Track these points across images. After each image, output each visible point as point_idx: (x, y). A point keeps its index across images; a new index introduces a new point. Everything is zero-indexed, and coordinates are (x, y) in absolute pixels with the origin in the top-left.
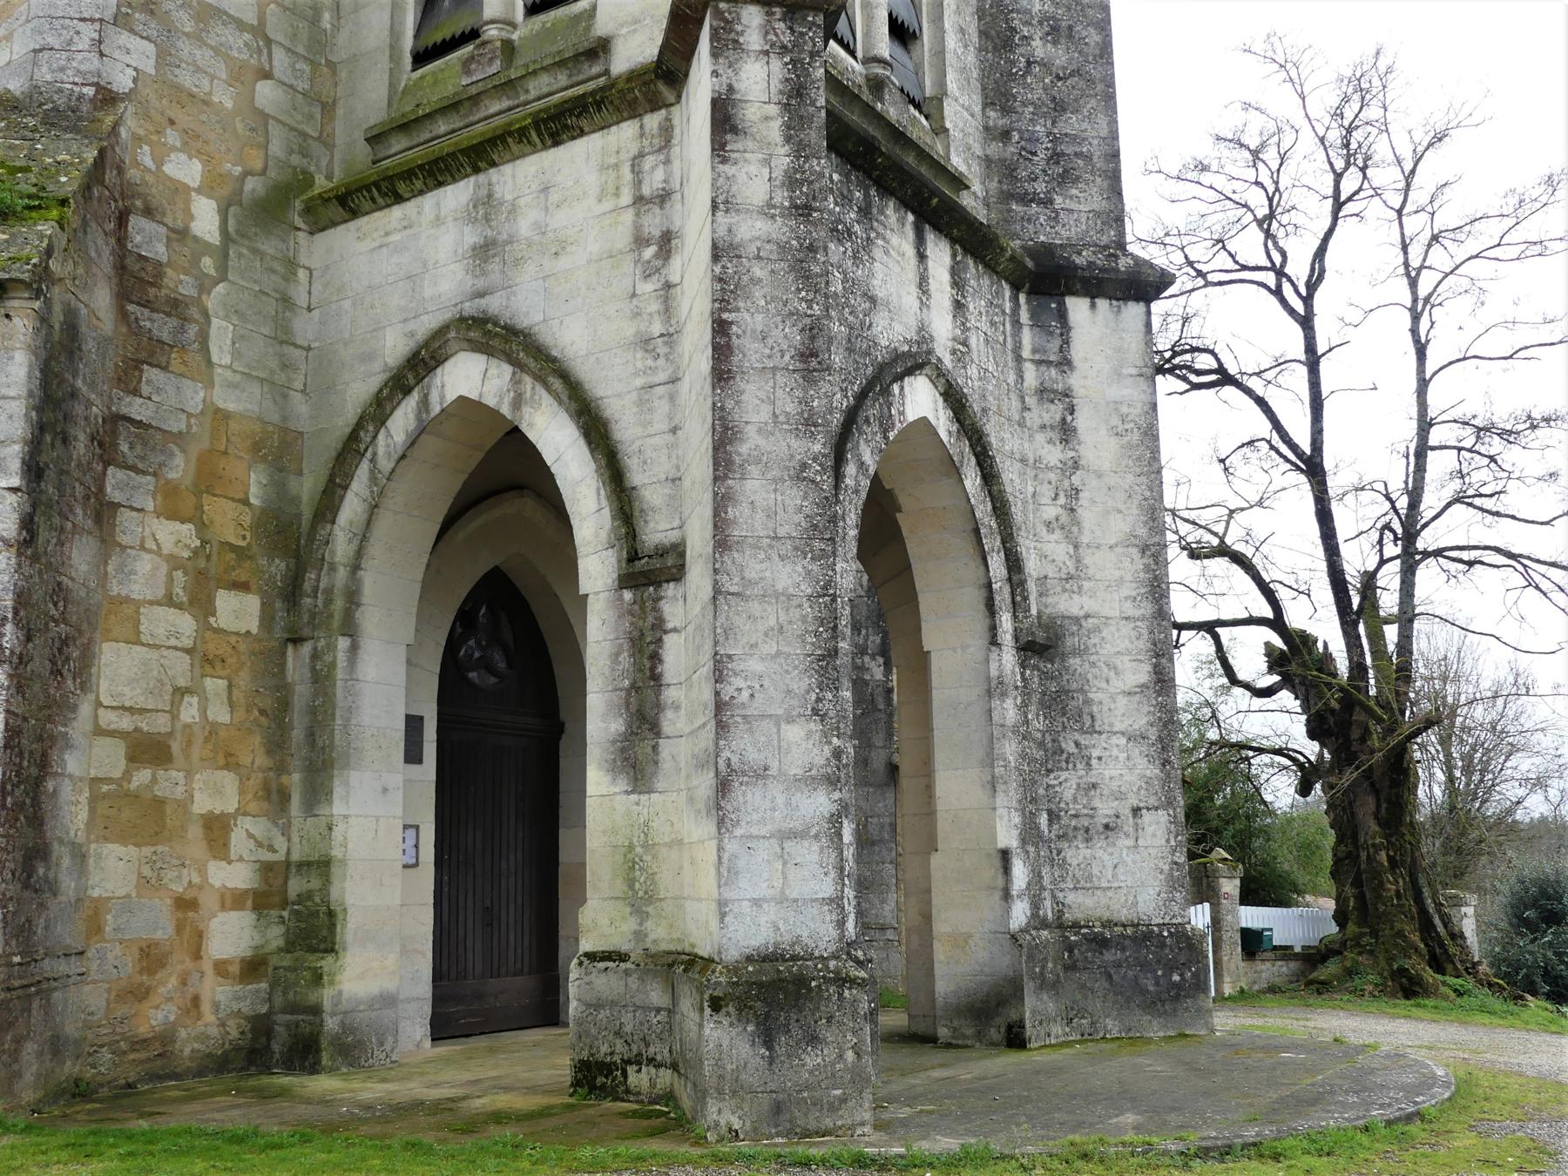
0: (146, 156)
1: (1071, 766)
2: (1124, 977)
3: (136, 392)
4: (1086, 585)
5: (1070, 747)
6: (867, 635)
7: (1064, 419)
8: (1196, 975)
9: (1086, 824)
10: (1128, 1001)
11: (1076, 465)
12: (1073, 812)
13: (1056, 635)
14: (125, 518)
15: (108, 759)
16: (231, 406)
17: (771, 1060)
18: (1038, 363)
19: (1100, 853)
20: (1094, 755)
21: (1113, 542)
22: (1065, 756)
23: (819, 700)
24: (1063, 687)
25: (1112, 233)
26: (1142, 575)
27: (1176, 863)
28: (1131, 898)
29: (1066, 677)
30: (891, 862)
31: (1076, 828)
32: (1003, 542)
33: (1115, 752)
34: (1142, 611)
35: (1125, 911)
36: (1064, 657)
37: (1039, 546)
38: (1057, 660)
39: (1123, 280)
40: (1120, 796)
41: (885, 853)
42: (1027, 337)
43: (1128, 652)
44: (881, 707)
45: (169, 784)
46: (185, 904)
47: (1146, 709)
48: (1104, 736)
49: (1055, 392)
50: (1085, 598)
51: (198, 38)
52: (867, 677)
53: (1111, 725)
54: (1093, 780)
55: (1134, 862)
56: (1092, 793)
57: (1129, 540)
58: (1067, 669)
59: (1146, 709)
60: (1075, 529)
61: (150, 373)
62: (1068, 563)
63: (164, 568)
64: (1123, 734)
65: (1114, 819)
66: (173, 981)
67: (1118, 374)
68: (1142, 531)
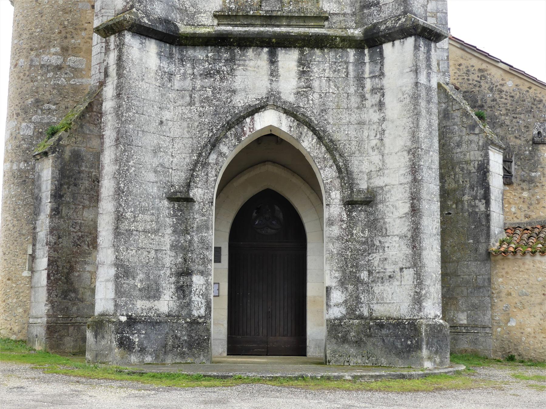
1: (377, 251)
2: (389, 341)
4: (386, 172)
5: (377, 243)
6: (477, 190)
7: (380, 100)
8: (417, 342)
9: (382, 276)
10: (390, 352)
11: (384, 119)
12: (377, 271)
13: (374, 195)
17: (96, 342)
18: (371, 78)
19: (387, 288)
20: (386, 246)
21: (397, 151)
22: (375, 247)
23: (114, 242)
24: (375, 218)
25: (402, 8)
26: (408, 163)
27: (416, 292)
28: (398, 308)
29: (377, 213)
30: (489, 296)
31: (378, 278)
32: (334, 162)
33: (394, 244)
34: (407, 180)
35: (395, 313)
36: (376, 204)
37: (369, 158)
38: (374, 206)
39: (398, 31)
41: (485, 292)
42: (367, 68)
43: (401, 199)
44: (484, 223)
47: (407, 223)
48: (390, 237)
49: (377, 89)
50: (385, 178)
52: (477, 210)
53: (393, 232)
54: (385, 257)
55: (400, 292)
56: (385, 262)
58: (377, 209)
59: (407, 223)
60: (382, 148)
62: (380, 164)
64: (398, 236)
65: (393, 273)
67: (402, 73)
68: (409, 143)
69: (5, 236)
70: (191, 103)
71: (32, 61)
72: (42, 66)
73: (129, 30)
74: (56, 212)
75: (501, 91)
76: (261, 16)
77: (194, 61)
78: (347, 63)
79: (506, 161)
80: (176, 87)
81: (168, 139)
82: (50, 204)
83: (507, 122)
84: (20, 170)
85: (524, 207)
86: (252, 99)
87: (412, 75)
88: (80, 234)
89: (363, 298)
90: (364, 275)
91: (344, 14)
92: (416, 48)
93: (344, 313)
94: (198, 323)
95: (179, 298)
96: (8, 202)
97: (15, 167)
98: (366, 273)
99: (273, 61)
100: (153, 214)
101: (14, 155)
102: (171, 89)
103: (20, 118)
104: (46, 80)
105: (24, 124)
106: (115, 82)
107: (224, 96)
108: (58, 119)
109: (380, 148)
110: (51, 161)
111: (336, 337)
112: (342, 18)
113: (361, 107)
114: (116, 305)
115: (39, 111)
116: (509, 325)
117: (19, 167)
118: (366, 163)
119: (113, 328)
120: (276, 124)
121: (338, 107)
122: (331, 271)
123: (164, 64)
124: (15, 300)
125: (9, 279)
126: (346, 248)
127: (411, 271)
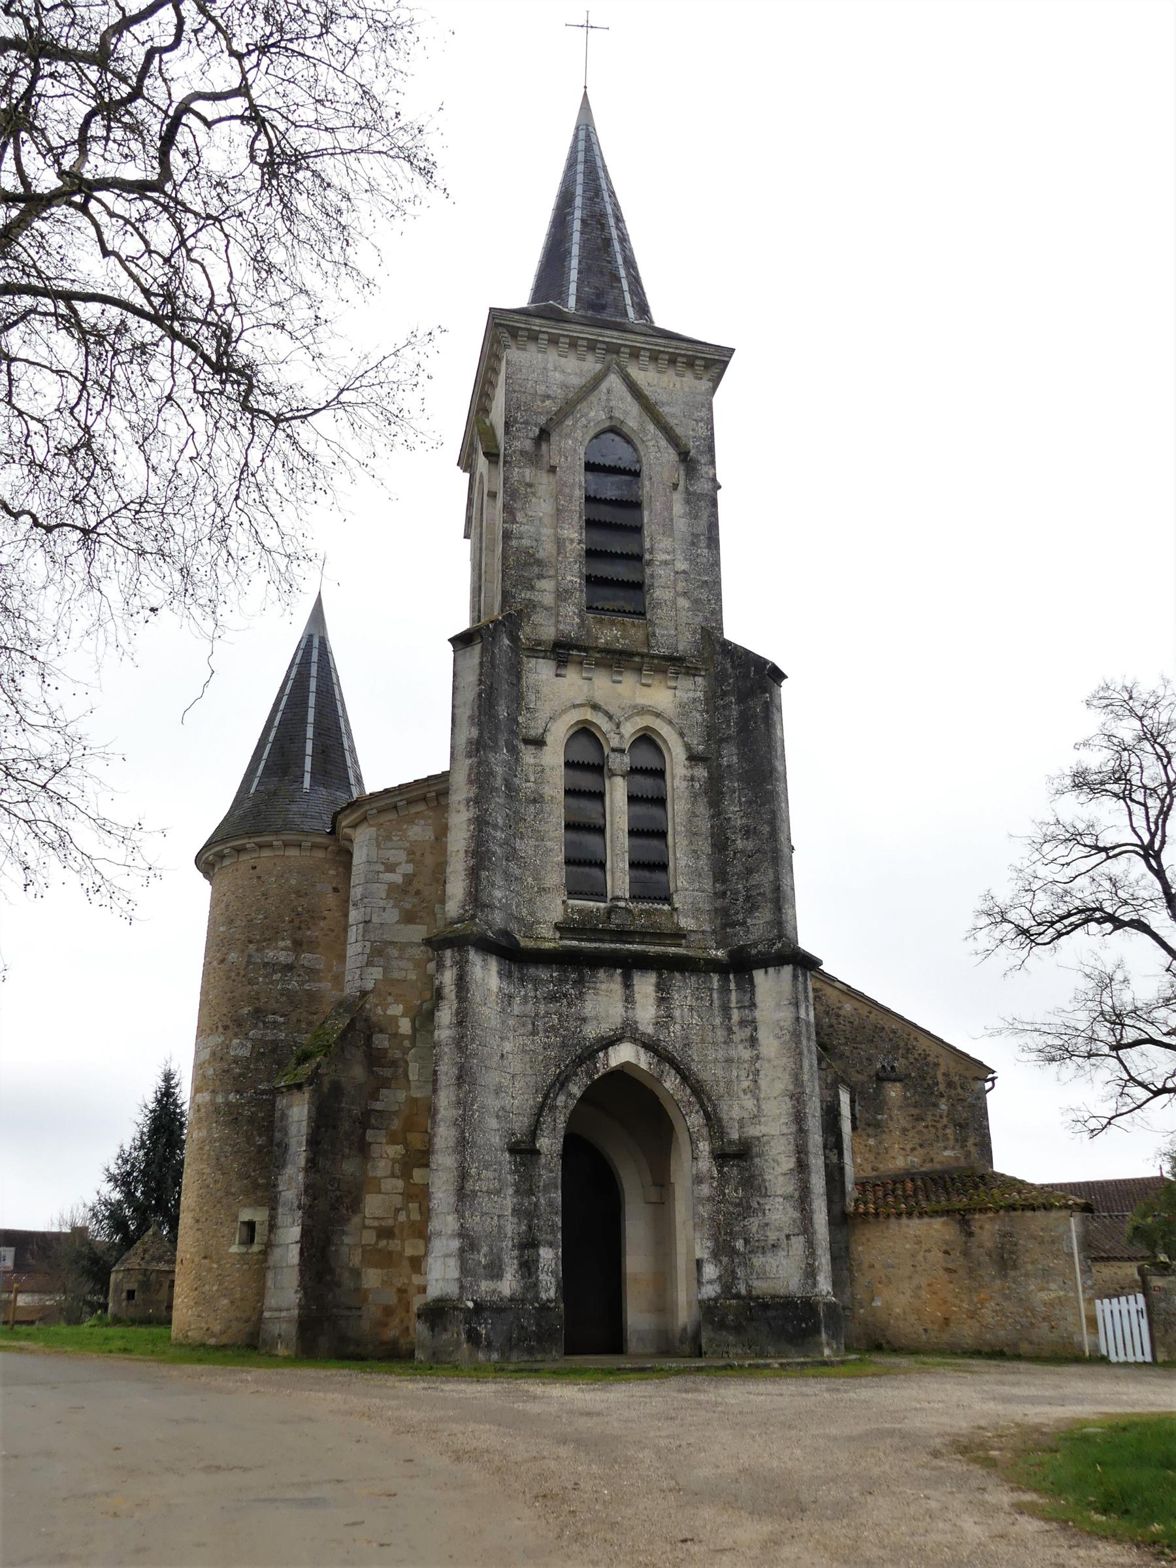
0: (379, 1011)
3: (377, 1100)
4: (763, 1119)
5: (755, 1205)
11: (758, 1057)
14: (374, 1147)
15: (369, 1237)
16: (419, 1096)
18: (739, 1008)
19: (770, 1260)
36: (752, 1158)
40: (780, 1229)
42: (734, 996)
45: (394, 1245)
46: (402, 1291)
47: (793, 1181)
51: (401, 958)
57: (785, 1093)
61: (384, 1091)
63: (390, 1163)
66: (397, 1321)
67: (778, 1005)
68: (791, 1087)
69: (199, 1196)
70: (534, 1033)
71: (250, 956)
72: (266, 965)
73: (473, 945)
74: (312, 1165)
75: (838, 1016)
76: (611, 931)
77: (537, 982)
78: (711, 990)
79: (852, 1101)
80: (516, 1013)
81: (508, 1077)
82: (304, 1154)
83: (847, 1054)
84: (228, 1104)
85: (871, 1157)
86: (604, 1029)
87: (792, 1009)
88: (338, 1193)
89: (740, 1272)
90: (739, 1244)
91: (703, 932)
92: (795, 977)
93: (719, 1291)
94: (549, 1309)
95: (523, 1278)
96: (207, 1148)
97: (220, 1099)
98: (741, 1241)
99: (628, 985)
100: (495, 1170)
101: (218, 1083)
102: (510, 1015)
103: (230, 1033)
104: (272, 983)
105: (236, 1041)
106: (455, 1006)
107: (572, 1024)
108: (287, 1035)
109: (754, 1090)
110: (307, 1095)
111: (712, 1323)
112: (700, 936)
113: (728, 1042)
114: (462, 1287)
115: (261, 1025)
116: (874, 1304)
117: (227, 1099)
118: (736, 1108)
119: (461, 1316)
120: (633, 1061)
121: (703, 1041)
122: (702, 1239)
123: (504, 985)
124: (215, 1288)
125: (205, 1258)
126: (718, 1212)
127: (801, 1239)
